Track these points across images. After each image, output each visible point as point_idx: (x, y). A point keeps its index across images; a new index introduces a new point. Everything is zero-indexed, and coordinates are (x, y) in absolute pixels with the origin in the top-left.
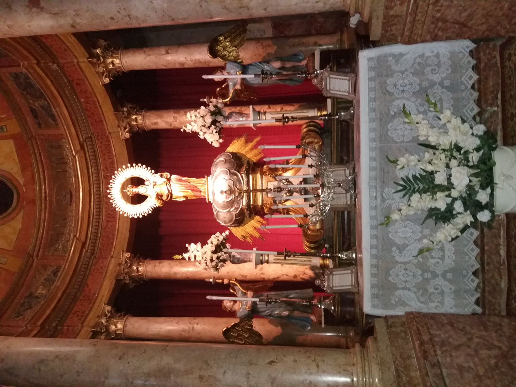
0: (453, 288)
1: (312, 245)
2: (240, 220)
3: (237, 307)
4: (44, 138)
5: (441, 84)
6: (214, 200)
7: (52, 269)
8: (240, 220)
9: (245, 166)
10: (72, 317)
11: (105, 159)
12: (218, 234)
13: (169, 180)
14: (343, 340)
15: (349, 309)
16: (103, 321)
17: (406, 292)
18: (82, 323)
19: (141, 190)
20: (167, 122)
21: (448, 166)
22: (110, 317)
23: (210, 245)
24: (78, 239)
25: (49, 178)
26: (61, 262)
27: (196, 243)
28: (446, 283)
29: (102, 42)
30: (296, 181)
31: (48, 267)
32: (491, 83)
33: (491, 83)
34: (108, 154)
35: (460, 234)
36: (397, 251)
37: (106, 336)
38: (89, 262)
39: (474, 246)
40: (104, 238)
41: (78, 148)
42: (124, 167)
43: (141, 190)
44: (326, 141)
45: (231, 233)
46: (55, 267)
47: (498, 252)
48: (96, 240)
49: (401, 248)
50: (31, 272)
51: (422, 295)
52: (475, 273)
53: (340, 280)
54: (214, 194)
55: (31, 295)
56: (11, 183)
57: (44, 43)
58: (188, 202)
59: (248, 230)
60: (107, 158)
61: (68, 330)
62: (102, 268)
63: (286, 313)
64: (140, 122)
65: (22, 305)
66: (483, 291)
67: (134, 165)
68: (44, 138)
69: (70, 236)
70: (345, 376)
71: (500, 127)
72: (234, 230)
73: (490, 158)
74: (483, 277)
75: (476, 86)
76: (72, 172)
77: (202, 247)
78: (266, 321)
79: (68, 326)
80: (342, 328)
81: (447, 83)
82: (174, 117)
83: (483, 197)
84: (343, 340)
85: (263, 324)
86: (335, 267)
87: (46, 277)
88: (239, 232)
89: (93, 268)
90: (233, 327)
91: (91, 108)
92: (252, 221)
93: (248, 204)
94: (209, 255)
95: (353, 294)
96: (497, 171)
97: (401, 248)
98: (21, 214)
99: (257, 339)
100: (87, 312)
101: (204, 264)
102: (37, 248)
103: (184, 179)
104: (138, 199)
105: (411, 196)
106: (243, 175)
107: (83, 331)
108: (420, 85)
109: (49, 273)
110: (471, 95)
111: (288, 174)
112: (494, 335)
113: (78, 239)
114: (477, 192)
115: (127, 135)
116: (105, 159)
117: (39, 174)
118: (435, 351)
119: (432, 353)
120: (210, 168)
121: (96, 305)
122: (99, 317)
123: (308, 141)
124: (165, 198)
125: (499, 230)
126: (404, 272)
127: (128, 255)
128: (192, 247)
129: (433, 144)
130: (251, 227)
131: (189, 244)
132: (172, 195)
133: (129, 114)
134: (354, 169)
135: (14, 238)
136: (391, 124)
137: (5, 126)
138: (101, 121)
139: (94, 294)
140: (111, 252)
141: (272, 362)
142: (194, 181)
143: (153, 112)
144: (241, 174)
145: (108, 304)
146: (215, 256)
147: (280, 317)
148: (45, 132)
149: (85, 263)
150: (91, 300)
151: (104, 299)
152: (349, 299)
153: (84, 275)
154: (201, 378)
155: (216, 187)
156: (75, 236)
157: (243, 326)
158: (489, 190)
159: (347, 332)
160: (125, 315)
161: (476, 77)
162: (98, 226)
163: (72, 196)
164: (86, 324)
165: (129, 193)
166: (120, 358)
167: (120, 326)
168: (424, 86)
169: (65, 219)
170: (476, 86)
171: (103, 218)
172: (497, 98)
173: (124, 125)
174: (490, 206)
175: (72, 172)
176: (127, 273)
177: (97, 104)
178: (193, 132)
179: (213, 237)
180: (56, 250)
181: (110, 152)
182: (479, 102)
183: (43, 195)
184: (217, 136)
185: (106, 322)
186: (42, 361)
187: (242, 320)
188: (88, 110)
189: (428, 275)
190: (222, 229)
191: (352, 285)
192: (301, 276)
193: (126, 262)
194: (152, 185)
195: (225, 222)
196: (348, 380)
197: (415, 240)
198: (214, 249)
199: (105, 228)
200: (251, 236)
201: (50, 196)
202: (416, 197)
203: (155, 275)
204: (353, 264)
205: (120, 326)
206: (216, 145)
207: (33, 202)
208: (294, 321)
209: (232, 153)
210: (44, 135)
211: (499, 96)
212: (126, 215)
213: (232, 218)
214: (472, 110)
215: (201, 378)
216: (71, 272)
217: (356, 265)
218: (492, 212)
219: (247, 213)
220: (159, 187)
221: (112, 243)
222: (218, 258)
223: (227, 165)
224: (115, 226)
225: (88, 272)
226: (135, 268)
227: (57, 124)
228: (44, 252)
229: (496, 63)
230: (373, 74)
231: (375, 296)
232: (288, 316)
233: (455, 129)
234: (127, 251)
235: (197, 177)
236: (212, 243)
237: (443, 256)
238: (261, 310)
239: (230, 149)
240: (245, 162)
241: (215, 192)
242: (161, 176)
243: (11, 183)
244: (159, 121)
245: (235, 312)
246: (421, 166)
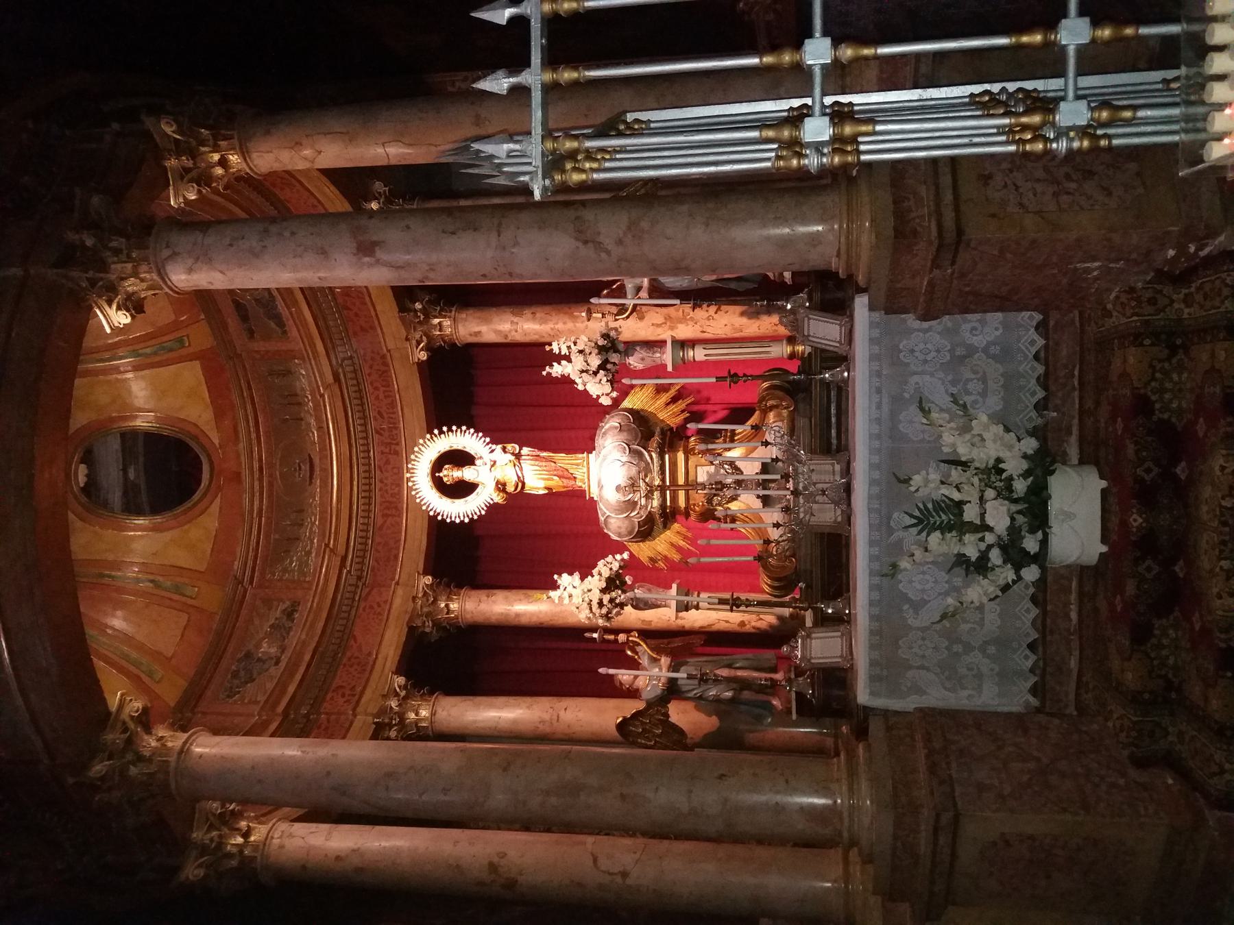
0: (997, 669)
1: (776, 584)
2: (646, 531)
3: (640, 683)
4: (258, 356)
5: (985, 350)
6: (601, 497)
7: (282, 607)
8: (646, 531)
9: (657, 438)
10: (332, 698)
11: (377, 398)
12: (610, 559)
13: (518, 456)
14: (830, 742)
15: (836, 692)
16: (394, 704)
17: (923, 672)
18: (354, 710)
19: (468, 474)
20: (498, 332)
21: (982, 499)
22: (405, 698)
23: (597, 577)
24: (332, 550)
25: (265, 433)
26: (300, 593)
27: (571, 574)
28: (987, 661)
29: (379, 186)
30: (750, 469)
31: (275, 603)
32: (1064, 352)
33: (1064, 352)
34: (382, 389)
35: (1000, 594)
36: (911, 611)
37: (399, 731)
38: (355, 593)
39: (1030, 605)
40: (380, 548)
41: (330, 379)
42: (436, 431)
43: (468, 474)
44: (801, 406)
45: (631, 555)
46: (288, 603)
47: (1067, 616)
48: (365, 551)
49: (917, 606)
50: (244, 612)
51: (948, 678)
52: (1032, 647)
53: (821, 647)
54: (601, 487)
55: (248, 655)
56: (198, 442)
57: (275, 195)
58: (551, 494)
59: (659, 549)
60: (381, 396)
61: (328, 721)
62: (379, 606)
63: (729, 694)
64: (448, 331)
65: (235, 675)
66: (1043, 676)
67: (454, 428)
68: (258, 356)
69: (312, 543)
70: (825, 796)
71: (1076, 421)
72: (634, 547)
73: (1045, 487)
74: (1045, 652)
75: (1042, 354)
76: (313, 421)
77: (582, 579)
78: (689, 706)
79: (327, 714)
80: (828, 721)
81: (995, 350)
82: (512, 322)
83: (1031, 544)
84: (830, 742)
85: (685, 712)
86: (816, 624)
87: (273, 621)
88: (644, 551)
89: (362, 604)
90: (636, 715)
91: (354, 304)
92: (668, 533)
93: (663, 506)
94: (596, 596)
95: (845, 670)
96: (1054, 506)
97: (917, 606)
98: (218, 500)
99: (675, 738)
100: (359, 689)
101: (588, 611)
102: (250, 563)
103: (545, 454)
104: (463, 489)
105: (928, 535)
106: (654, 455)
107: (358, 723)
108: (952, 351)
109: (278, 614)
110: (1033, 369)
111: (736, 453)
112: (1034, 741)
113: (332, 550)
114: (1023, 538)
115: (423, 356)
116: (377, 398)
117: (248, 422)
118: (948, 764)
119: (944, 766)
120: (592, 439)
121: (375, 675)
122: (385, 697)
123: (770, 403)
124: (510, 489)
125: (1070, 581)
126: (920, 642)
127: (428, 580)
128: (565, 580)
129: (963, 459)
130: (664, 544)
131: (560, 575)
132: (523, 484)
133: (428, 317)
134: (849, 463)
135: (208, 547)
136: (904, 413)
137: (188, 336)
138: (373, 328)
139: (370, 654)
140: (394, 574)
141: (723, 775)
142: (562, 459)
143: (471, 311)
144: (649, 452)
145: (398, 672)
146: (606, 598)
147: (717, 700)
148: (259, 346)
149: (347, 595)
150: (366, 667)
151: (388, 664)
152: (835, 679)
153: (348, 619)
154: (623, 797)
155: (606, 472)
156: (327, 545)
157: (651, 716)
158: (1040, 535)
159: (837, 727)
160: (431, 693)
161: (1041, 342)
162: (367, 524)
163: (313, 468)
164: (359, 710)
165: (445, 479)
166: (505, 770)
167: (424, 713)
168: (958, 353)
169: (301, 511)
170: (1042, 354)
171: (377, 509)
172: (1073, 376)
173: (418, 336)
174: (1039, 558)
175: (313, 421)
176: (428, 615)
177: (367, 299)
178: (563, 376)
179: (601, 563)
180: (285, 570)
181: (388, 385)
182: (1044, 382)
183: (256, 465)
184: (608, 388)
185: (399, 705)
186: (389, 775)
187: (650, 704)
188: (348, 309)
189: (958, 648)
190: (619, 548)
191: (841, 657)
192: (753, 624)
193: (425, 594)
194: (488, 466)
195: (620, 535)
196: (830, 802)
197: (940, 594)
198: (604, 585)
199: (381, 528)
200: (666, 558)
201: (271, 466)
202: (935, 537)
203: (480, 619)
204: (841, 621)
205: (424, 713)
206: (605, 401)
207: (237, 477)
208: (743, 707)
209: (631, 411)
210: (257, 352)
211: (1076, 373)
212: (439, 518)
213: (633, 529)
214: (1034, 394)
215: (623, 797)
216: (324, 615)
217: (849, 622)
218: (1043, 568)
219: (659, 521)
220: (500, 469)
221: (396, 557)
222: (612, 601)
223: (624, 436)
224: (399, 524)
225: (353, 612)
226: (443, 605)
227: (285, 332)
228: (263, 574)
229: (1073, 321)
230: (876, 333)
231: (873, 679)
232: (732, 701)
233: (995, 441)
234: (425, 573)
235: (569, 451)
236: (600, 574)
237: (983, 619)
238: (684, 689)
239: (627, 403)
240: (658, 430)
241: (603, 482)
242: (504, 450)
243: (198, 442)
244: (484, 329)
245: (637, 690)
246: (945, 491)
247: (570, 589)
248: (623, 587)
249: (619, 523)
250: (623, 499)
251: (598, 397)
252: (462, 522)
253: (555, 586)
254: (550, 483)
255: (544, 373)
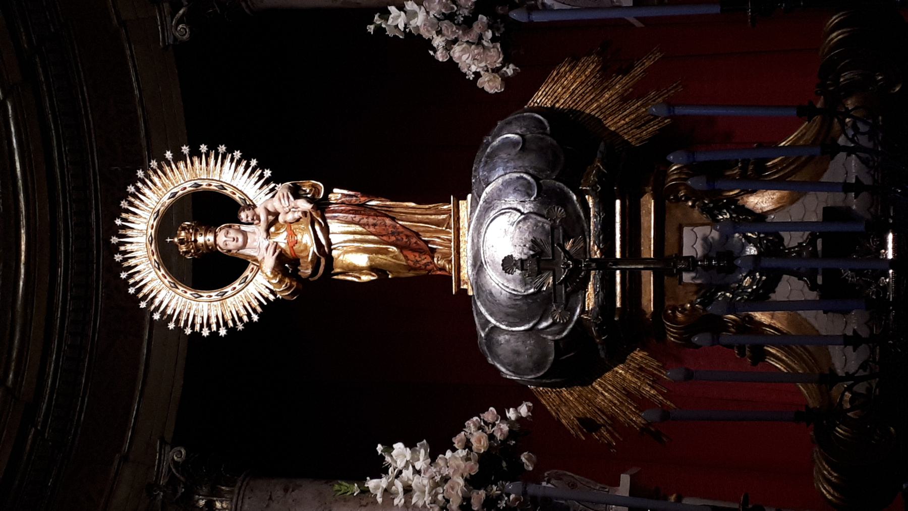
2: (576, 359)
6: (479, 285)
12: (491, 414)
13: (321, 206)
19: (225, 239)
43: (225, 239)
72: (549, 397)
77: (433, 457)
88: (567, 404)
124: (306, 271)
130: (616, 387)
184: (495, 57)
206: (491, 85)
226: (202, 503)
236: (468, 445)
239: (540, 98)
247: (408, 474)
248: (516, 472)
249: (515, 344)
250: (521, 290)
251: (477, 75)
252: (214, 335)
253: (379, 469)
254: (381, 259)
255: (371, 28)
